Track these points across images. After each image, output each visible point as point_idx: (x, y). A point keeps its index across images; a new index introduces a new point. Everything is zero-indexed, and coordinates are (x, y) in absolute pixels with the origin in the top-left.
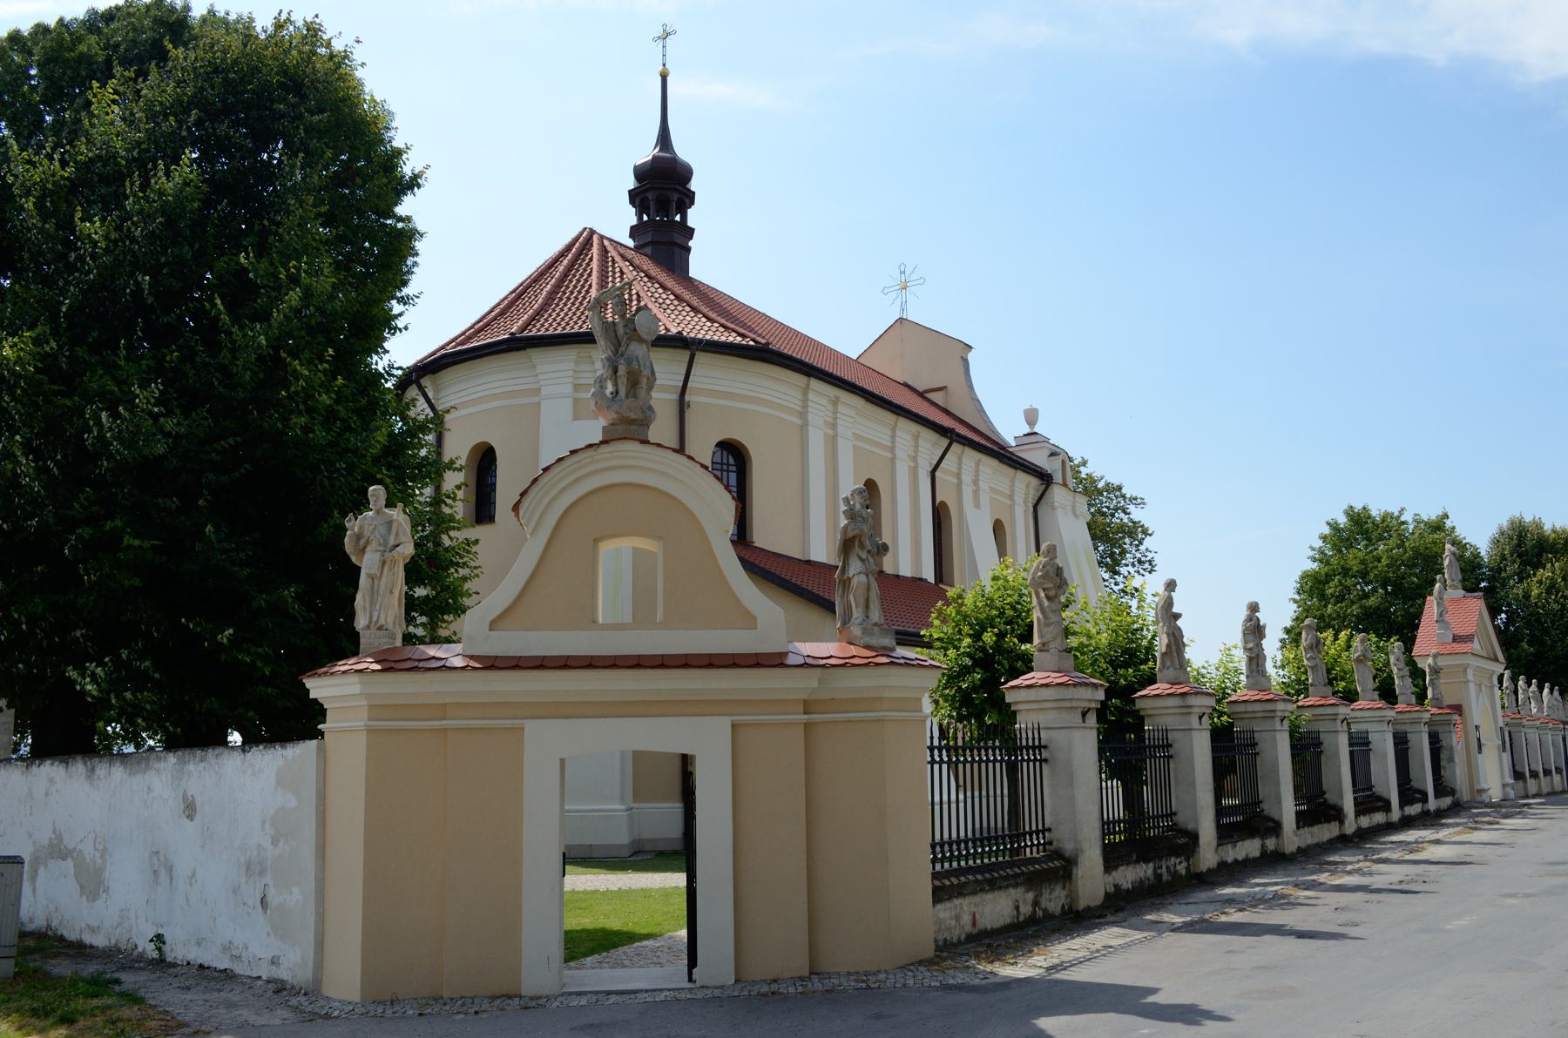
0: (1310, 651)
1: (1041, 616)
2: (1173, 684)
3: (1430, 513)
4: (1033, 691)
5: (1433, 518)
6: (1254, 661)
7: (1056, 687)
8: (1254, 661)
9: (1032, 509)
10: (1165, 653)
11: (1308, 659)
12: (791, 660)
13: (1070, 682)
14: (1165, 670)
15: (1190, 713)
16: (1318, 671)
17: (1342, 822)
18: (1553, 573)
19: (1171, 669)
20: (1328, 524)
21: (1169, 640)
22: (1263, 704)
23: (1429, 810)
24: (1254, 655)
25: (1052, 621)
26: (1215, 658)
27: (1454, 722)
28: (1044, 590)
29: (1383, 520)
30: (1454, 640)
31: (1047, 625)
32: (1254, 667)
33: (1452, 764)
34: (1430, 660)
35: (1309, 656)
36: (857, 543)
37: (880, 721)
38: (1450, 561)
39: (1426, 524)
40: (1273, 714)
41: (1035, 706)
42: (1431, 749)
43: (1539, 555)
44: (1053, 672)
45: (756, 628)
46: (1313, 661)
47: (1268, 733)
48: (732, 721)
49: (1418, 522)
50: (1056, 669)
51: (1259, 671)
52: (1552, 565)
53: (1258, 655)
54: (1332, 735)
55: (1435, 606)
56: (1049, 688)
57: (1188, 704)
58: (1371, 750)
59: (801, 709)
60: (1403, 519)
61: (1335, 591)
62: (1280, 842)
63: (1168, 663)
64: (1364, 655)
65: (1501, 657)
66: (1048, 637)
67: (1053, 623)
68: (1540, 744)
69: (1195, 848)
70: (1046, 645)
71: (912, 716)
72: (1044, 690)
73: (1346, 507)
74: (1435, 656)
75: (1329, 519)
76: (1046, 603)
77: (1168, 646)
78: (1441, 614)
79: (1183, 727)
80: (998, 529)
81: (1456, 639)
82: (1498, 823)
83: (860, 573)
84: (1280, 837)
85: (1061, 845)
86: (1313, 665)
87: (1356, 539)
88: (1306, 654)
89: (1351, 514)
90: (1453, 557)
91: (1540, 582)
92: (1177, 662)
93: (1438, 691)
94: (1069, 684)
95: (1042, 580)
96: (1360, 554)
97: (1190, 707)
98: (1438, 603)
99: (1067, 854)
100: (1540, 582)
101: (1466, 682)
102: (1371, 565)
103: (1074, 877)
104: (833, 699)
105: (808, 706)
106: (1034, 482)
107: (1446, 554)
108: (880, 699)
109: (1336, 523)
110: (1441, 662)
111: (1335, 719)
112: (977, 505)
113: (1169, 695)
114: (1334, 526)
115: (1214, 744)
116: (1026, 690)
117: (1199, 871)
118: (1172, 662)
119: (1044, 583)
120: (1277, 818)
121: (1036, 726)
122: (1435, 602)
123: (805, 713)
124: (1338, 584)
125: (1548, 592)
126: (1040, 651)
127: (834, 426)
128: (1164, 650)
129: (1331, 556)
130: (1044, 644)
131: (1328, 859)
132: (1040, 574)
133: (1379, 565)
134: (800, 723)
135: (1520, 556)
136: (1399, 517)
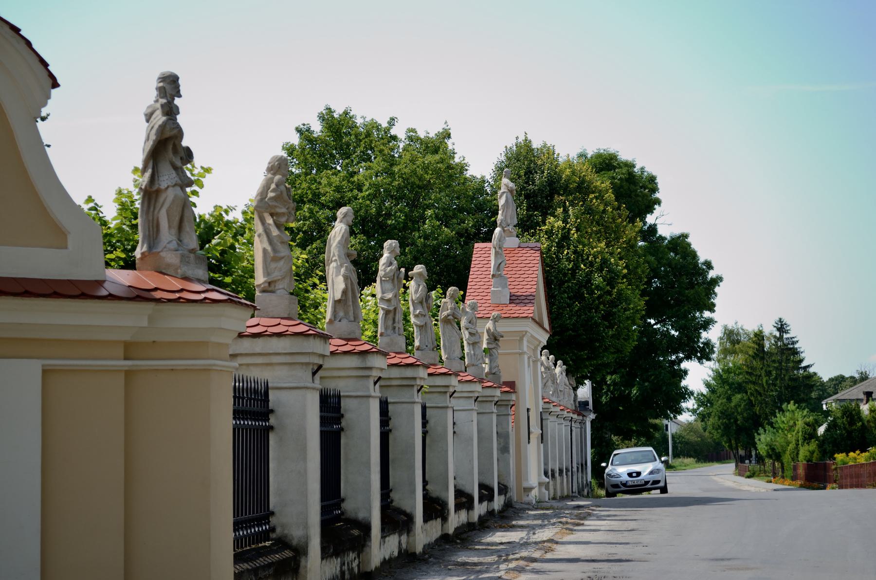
0: (419, 306)
1: (269, 248)
2: (348, 340)
3: (428, 129)
4: (260, 341)
5: (432, 135)
6: (391, 316)
7: (293, 338)
8: (391, 316)
10: (339, 301)
11: (416, 316)
12: (108, 289)
13: (311, 332)
14: (337, 322)
15: (368, 377)
16: (426, 331)
17: (445, 519)
18: (565, 221)
19: (344, 322)
20: (298, 130)
21: (346, 285)
22: (403, 370)
23: (493, 510)
24: (391, 308)
25: (282, 254)
26: (731, 325)
27: (512, 403)
28: (272, 215)
29: (368, 135)
30: (512, 301)
31: (275, 259)
32: (390, 323)
33: (506, 454)
34: (490, 325)
35: (418, 312)
36: (170, 147)
37: (206, 370)
38: (507, 201)
39: (422, 142)
40: (412, 383)
41: (260, 360)
42: (323, 434)
43: (551, 196)
44: (282, 318)
45: (66, 248)
46: (422, 319)
47: (405, 405)
48: (43, 366)
49: (413, 138)
50: (286, 316)
51: (394, 328)
52: (566, 211)
53: (395, 309)
54: (440, 411)
55: (492, 258)
56: (282, 339)
57: (369, 364)
58: (271, 428)
59: (121, 352)
60: (393, 132)
61: (304, 225)
62: (411, 539)
63: (341, 314)
64: (453, 315)
65: (546, 325)
66: (276, 275)
67: (283, 258)
68: (425, 434)
69: (365, 541)
70: (273, 286)
71: (193, 365)
72: (275, 340)
73: (322, 109)
74: (496, 320)
75: (299, 123)
76: (275, 232)
77: (344, 292)
78: (498, 267)
79: (359, 394)
81: (514, 299)
82: (583, 524)
83: (176, 185)
84: (411, 534)
85: (286, 532)
86: (422, 324)
87: (332, 156)
88: (414, 309)
89: (327, 118)
90: (509, 194)
91: (550, 233)
92: (351, 313)
93: (495, 364)
94: (311, 335)
95: (275, 203)
96: (336, 180)
97: (370, 368)
98: (497, 253)
99: (295, 543)
100: (550, 233)
101: (521, 354)
102: (349, 194)
103: (302, 570)
104: (154, 342)
105: (130, 350)
107: (502, 190)
108: (205, 344)
109: (308, 130)
110: (503, 327)
111: (446, 392)
113: (345, 353)
114: (304, 132)
115: (323, 414)
116: (250, 340)
117: (369, 570)
118: (346, 313)
119: (276, 207)
120: (408, 511)
121: (266, 382)
122: (493, 252)
123: (126, 358)
124: (307, 214)
125: (560, 246)
126: (264, 291)
128: (338, 296)
129: (298, 176)
130: (270, 283)
131: (459, 560)
132: (271, 194)
133: (360, 195)
134: (121, 371)
135: (527, 197)
136: (387, 130)
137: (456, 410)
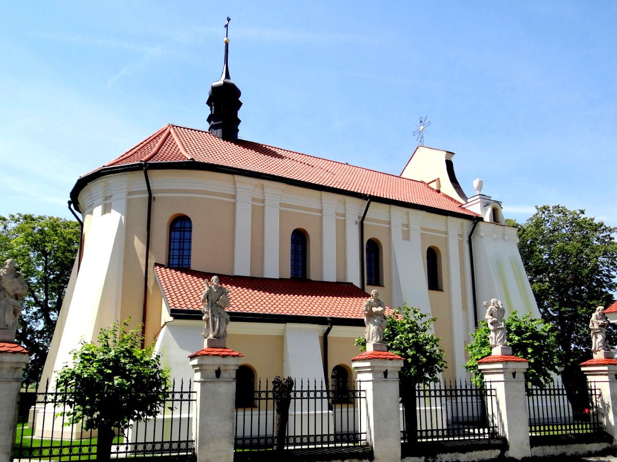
9: (468, 239)
80: (433, 257)
106: (467, 223)
112: (407, 236)
127: (407, 226)
137: (363, 381)
